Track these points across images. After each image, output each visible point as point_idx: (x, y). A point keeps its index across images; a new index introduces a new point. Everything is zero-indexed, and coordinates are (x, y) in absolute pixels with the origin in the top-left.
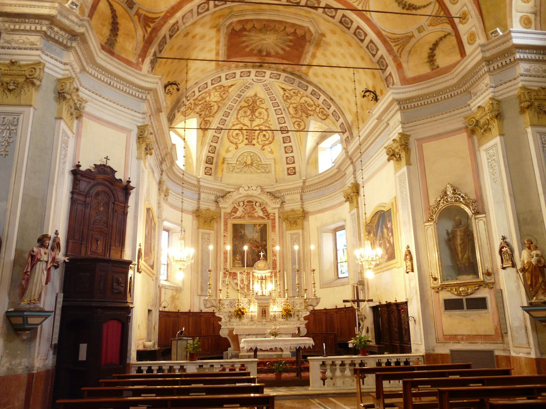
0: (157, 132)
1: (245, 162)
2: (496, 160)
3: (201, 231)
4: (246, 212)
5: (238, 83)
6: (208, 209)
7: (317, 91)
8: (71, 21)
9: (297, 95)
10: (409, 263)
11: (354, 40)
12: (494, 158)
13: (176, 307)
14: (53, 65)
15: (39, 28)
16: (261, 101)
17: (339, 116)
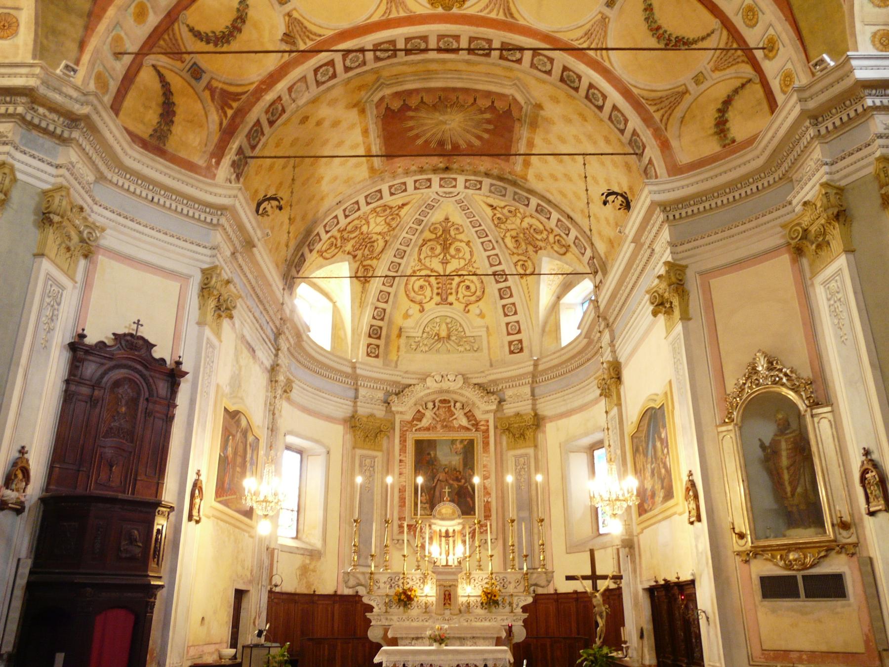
0: (257, 282)
1: (437, 334)
2: (842, 299)
3: (359, 452)
4: (438, 419)
5: (415, 201)
6: (372, 415)
7: (547, 204)
8: (66, 96)
9: (515, 216)
10: (693, 505)
11: (589, 110)
12: (839, 296)
13: (309, 585)
14: (34, 168)
15: (11, 110)
16: (457, 229)
17: (584, 247)
